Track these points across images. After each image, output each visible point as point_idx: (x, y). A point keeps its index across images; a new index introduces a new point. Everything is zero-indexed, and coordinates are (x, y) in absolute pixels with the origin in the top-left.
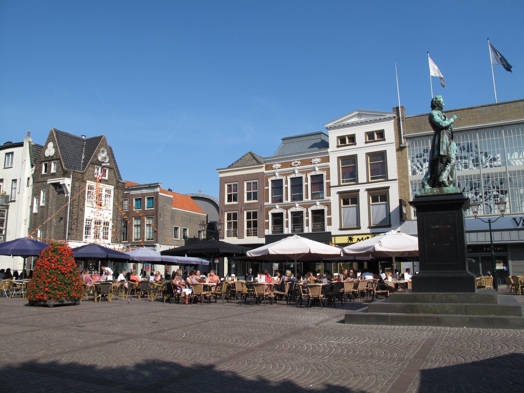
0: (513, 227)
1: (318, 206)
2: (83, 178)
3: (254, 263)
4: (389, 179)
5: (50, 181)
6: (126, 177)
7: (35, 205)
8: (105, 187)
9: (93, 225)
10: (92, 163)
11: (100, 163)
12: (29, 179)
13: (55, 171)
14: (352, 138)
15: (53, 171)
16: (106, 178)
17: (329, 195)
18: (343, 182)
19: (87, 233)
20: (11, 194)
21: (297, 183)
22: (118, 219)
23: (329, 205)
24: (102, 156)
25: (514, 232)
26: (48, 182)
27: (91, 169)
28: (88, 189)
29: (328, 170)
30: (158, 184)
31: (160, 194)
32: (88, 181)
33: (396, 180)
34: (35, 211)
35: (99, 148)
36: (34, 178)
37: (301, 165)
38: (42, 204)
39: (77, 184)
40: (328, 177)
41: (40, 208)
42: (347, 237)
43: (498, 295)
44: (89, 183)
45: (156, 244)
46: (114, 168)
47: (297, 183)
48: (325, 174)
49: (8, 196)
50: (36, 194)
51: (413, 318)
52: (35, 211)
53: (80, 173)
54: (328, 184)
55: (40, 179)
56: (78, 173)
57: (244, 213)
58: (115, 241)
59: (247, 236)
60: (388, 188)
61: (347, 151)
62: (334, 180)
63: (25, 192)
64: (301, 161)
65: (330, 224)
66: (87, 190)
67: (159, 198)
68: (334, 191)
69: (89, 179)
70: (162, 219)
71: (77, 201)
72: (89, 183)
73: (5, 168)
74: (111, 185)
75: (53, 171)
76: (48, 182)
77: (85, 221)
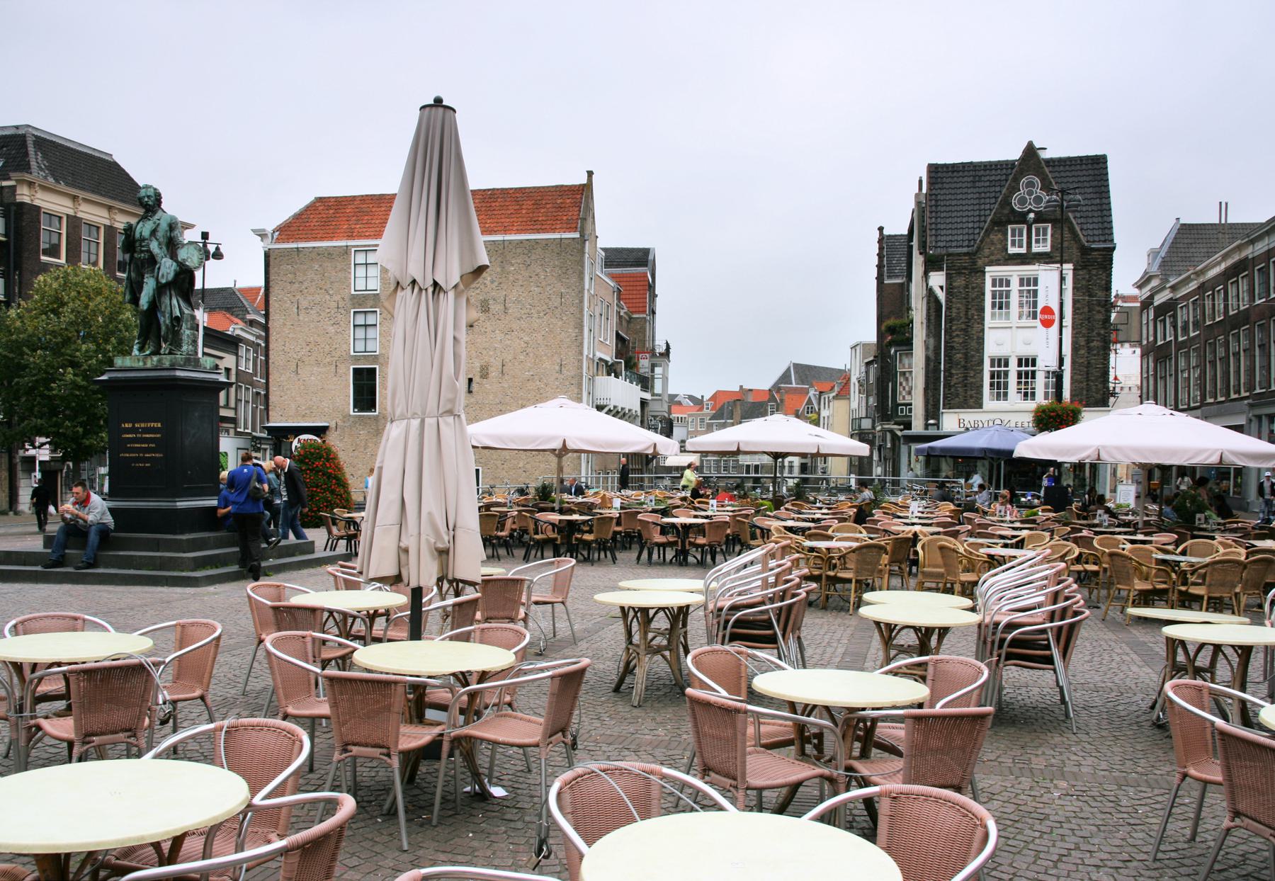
0: (1225, 662)
2: (974, 263)
9: (1013, 368)
12: (920, 182)
16: (1048, 249)
22: (1094, 344)
27: (996, 237)
33: (537, 603)
39: (959, 282)
44: (992, 272)
51: (290, 563)
53: (965, 254)
56: (959, 255)
69: (991, 264)
71: (963, 320)
72: (992, 272)
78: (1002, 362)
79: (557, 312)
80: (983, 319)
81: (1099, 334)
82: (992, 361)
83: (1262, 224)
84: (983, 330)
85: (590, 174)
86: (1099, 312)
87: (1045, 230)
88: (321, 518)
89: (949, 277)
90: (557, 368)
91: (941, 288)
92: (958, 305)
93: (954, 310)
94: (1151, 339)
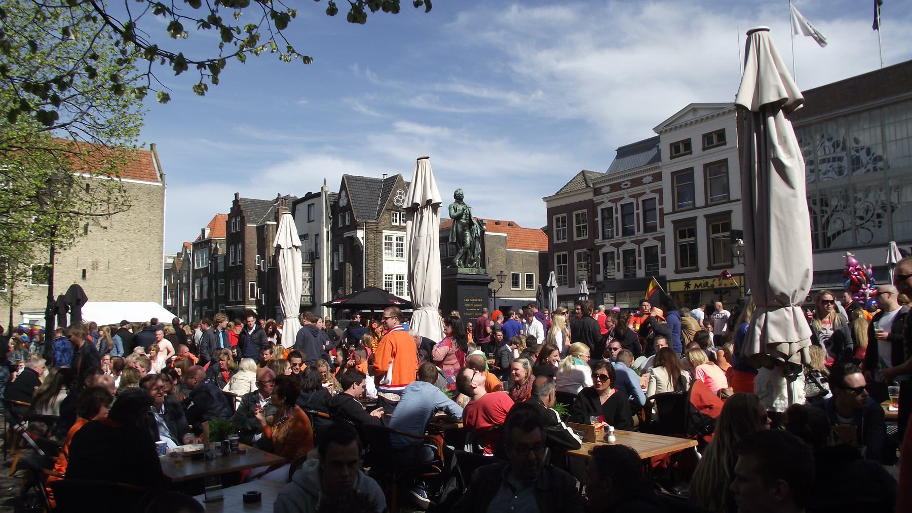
1: (651, 243)
4: (732, 198)
5: (346, 235)
7: (335, 263)
10: (387, 210)
14: (687, 144)
15: (347, 223)
17: (662, 226)
18: (679, 207)
21: (627, 211)
23: (662, 239)
29: (660, 191)
34: (336, 269)
35: (395, 191)
37: (632, 186)
39: (371, 236)
40: (661, 203)
42: (683, 283)
43: (35, 365)
44: (386, 233)
47: (627, 211)
48: (657, 196)
52: (336, 269)
54: (661, 210)
60: (730, 212)
61: (681, 164)
62: (668, 206)
64: (631, 181)
65: (664, 266)
66: (384, 241)
68: (668, 220)
70: (491, 265)
72: (386, 233)
73: (309, 222)
77: (384, 277)
78: (389, 276)
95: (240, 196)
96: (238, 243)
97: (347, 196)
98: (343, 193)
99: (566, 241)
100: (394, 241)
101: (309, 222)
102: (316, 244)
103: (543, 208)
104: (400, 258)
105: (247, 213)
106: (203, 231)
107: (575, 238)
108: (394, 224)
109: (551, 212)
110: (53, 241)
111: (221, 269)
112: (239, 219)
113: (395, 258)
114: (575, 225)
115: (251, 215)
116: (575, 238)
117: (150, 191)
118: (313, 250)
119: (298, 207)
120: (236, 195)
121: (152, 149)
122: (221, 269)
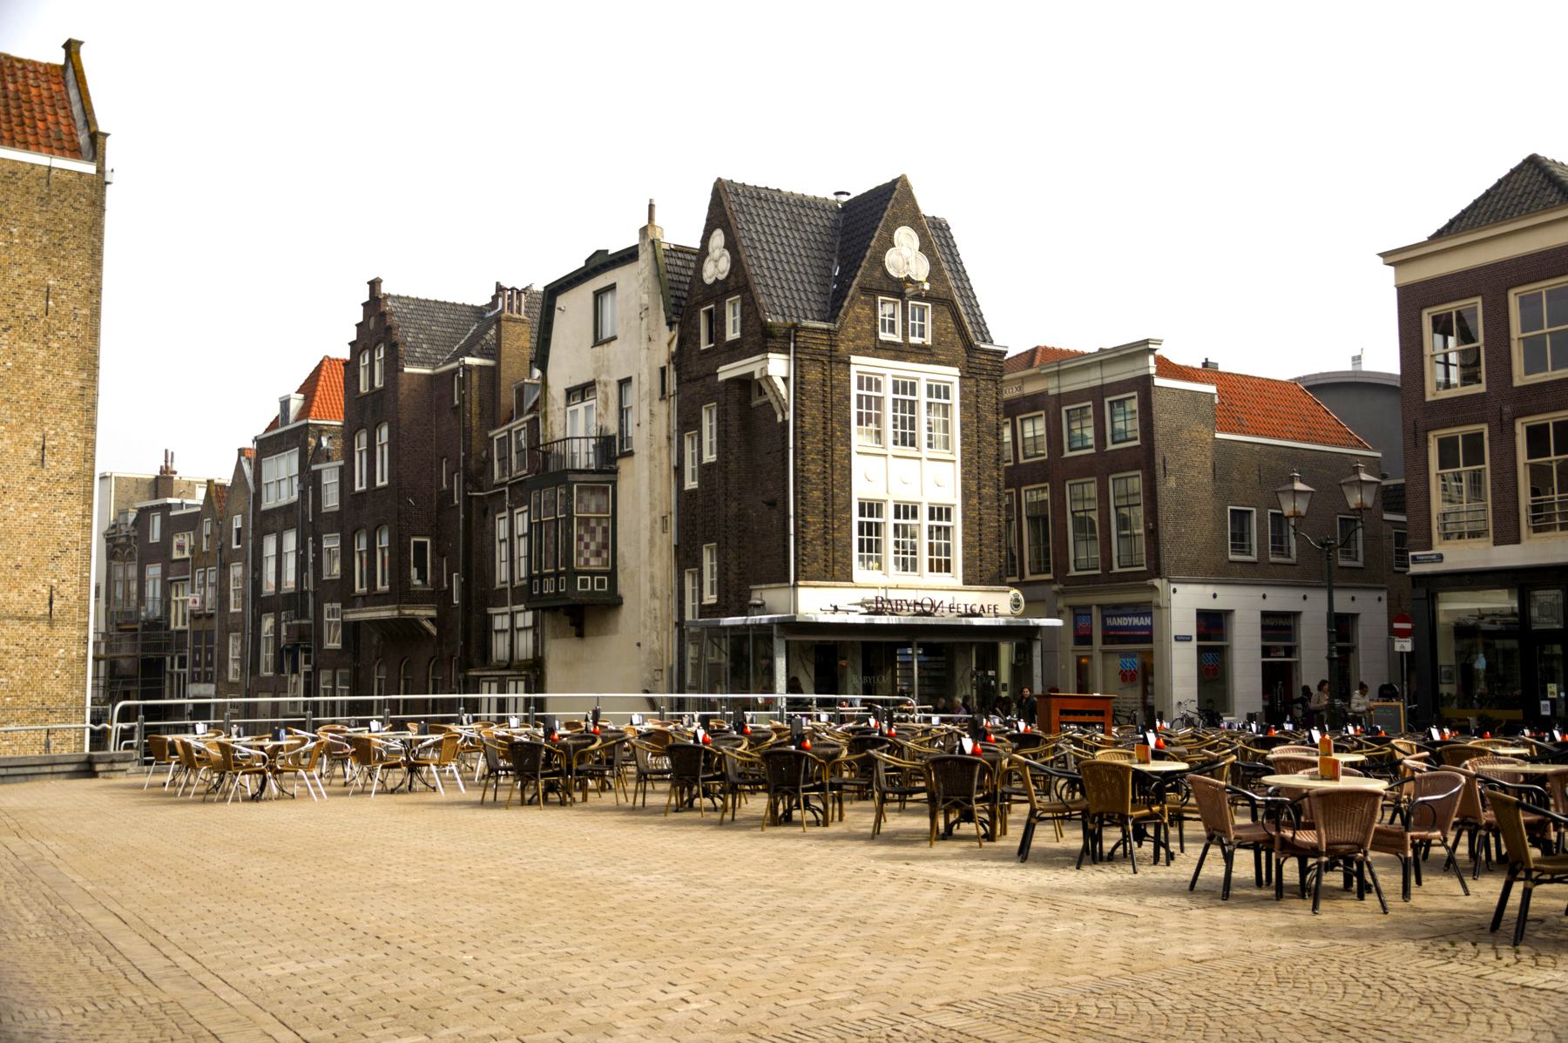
2: (833, 347)
3: (1499, 644)
5: (726, 372)
6: (1010, 333)
7: (689, 466)
8: (924, 374)
9: (888, 519)
11: (898, 288)
12: (663, 370)
13: (737, 335)
15: (732, 334)
16: (928, 340)
19: (871, 547)
20: (621, 432)
24: (905, 256)
25: (1253, 869)
26: (721, 377)
28: (860, 387)
30: (1146, 342)
31: (1158, 382)
32: (854, 359)
34: (691, 484)
36: (678, 369)
38: (709, 457)
41: (705, 471)
44: (861, 364)
45: (1157, 582)
46: (949, 296)
49: (614, 437)
50: (688, 422)
52: (691, 484)
53: (823, 331)
55: (696, 368)
57: (1514, 434)
58: (973, 578)
59: (1537, 530)
63: (650, 424)
67: (1156, 400)
72: (861, 364)
74: (949, 364)
75: (732, 334)
76: (721, 377)
78: (871, 508)
79: (37, 328)
80: (849, 438)
81: (991, 477)
82: (862, 506)
83: (1083, 354)
84: (849, 456)
85: (71, 47)
86: (990, 444)
87: (922, 309)
88: (1508, 710)
89: (799, 365)
90: (34, 454)
91: (785, 380)
92: (813, 411)
93: (807, 419)
94: (362, 544)
95: (385, 289)
96: (378, 425)
97: (731, 245)
98: (718, 238)
99: (1481, 388)
100: (887, 393)
101: (598, 341)
102: (622, 412)
103: (1383, 288)
104: (908, 451)
105: (407, 335)
106: (285, 404)
107: (1520, 378)
108: (884, 336)
109: (1411, 300)
110: (543, 719)
111: (331, 501)
112: (381, 354)
113: (892, 449)
114: (1516, 331)
115: (418, 343)
116: (1520, 378)
117: (50, 185)
118: (613, 429)
119: (562, 301)
120: (374, 285)
121: (68, 56)
122: (331, 501)
